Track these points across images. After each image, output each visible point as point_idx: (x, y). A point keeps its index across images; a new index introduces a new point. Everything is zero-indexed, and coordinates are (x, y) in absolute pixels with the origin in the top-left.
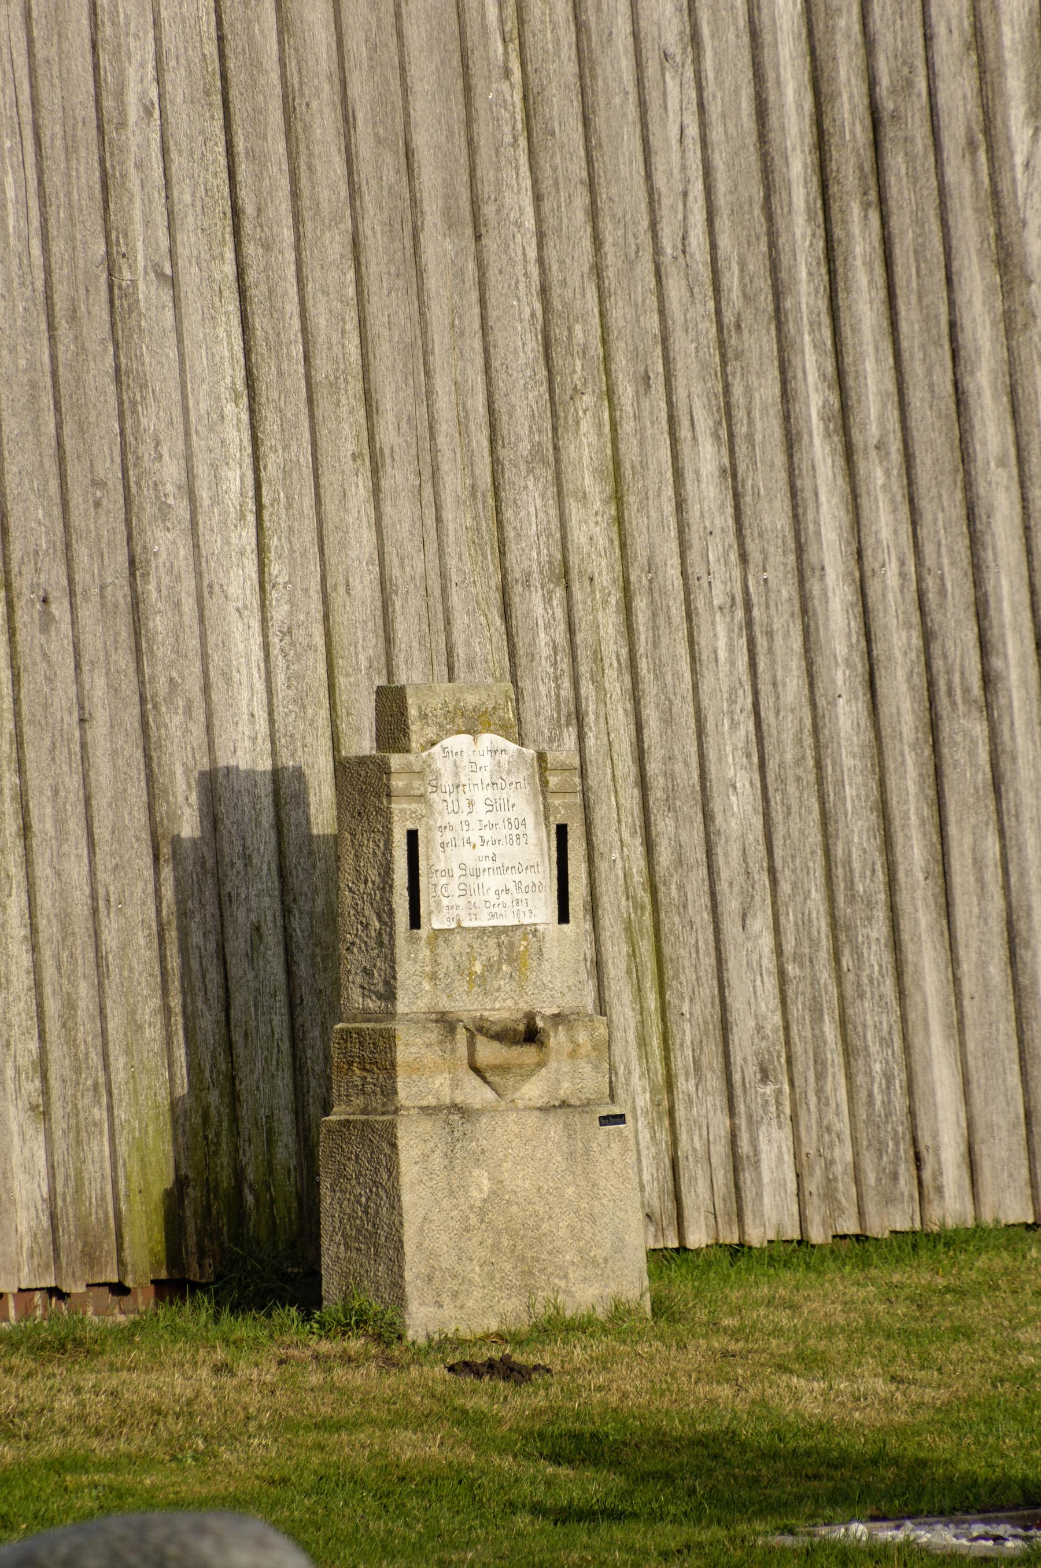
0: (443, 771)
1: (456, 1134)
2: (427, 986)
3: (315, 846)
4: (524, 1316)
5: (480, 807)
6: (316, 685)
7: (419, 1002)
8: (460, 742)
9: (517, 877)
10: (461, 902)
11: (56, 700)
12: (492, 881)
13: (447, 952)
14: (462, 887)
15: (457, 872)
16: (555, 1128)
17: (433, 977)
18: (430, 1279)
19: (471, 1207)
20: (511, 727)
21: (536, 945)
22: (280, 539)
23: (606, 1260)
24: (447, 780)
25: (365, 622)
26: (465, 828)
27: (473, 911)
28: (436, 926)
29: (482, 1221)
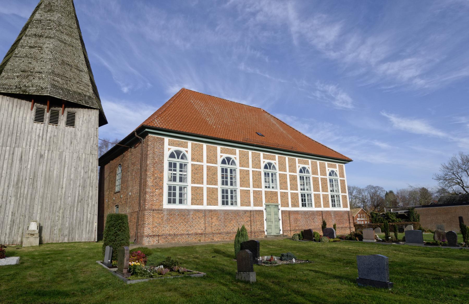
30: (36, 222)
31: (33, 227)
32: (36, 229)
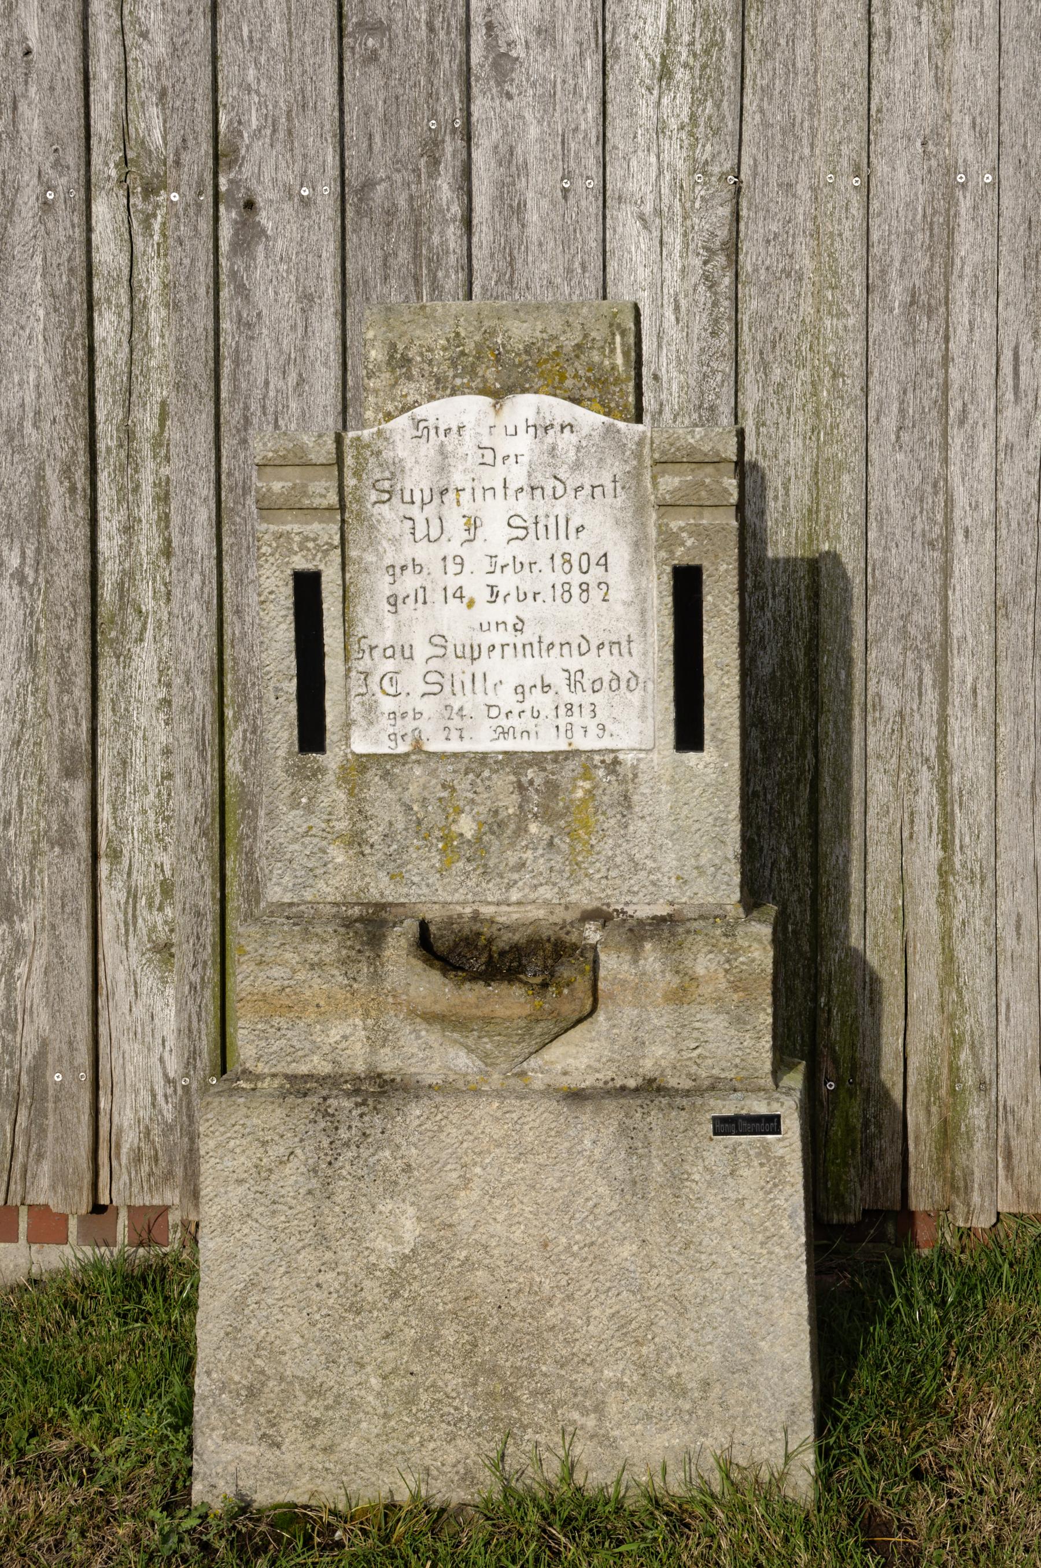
0: (409, 464)
1: (344, 1134)
2: (338, 855)
3: (766, 576)
4: (486, 1475)
5: (495, 533)
7: (321, 884)
8: (468, 409)
9: (574, 663)
10: (429, 706)
11: (257, 355)
12: (508, 671)
13: (389, 795)
14: (432, 678)
16: (595, 1134)
17: (356, 840)
18: (253, 1393)
19: (371, 1269)
20: (617, 381)
21: (615, 788)
22: (718, 105)
23: (706, 1385)
24: (418, 479)
25: (911, 235)
26: (452, 568)
28: (360, 745)
29: (396, 1295)
30: (626, 394)
31: (512, 611)
32: (634, 721)
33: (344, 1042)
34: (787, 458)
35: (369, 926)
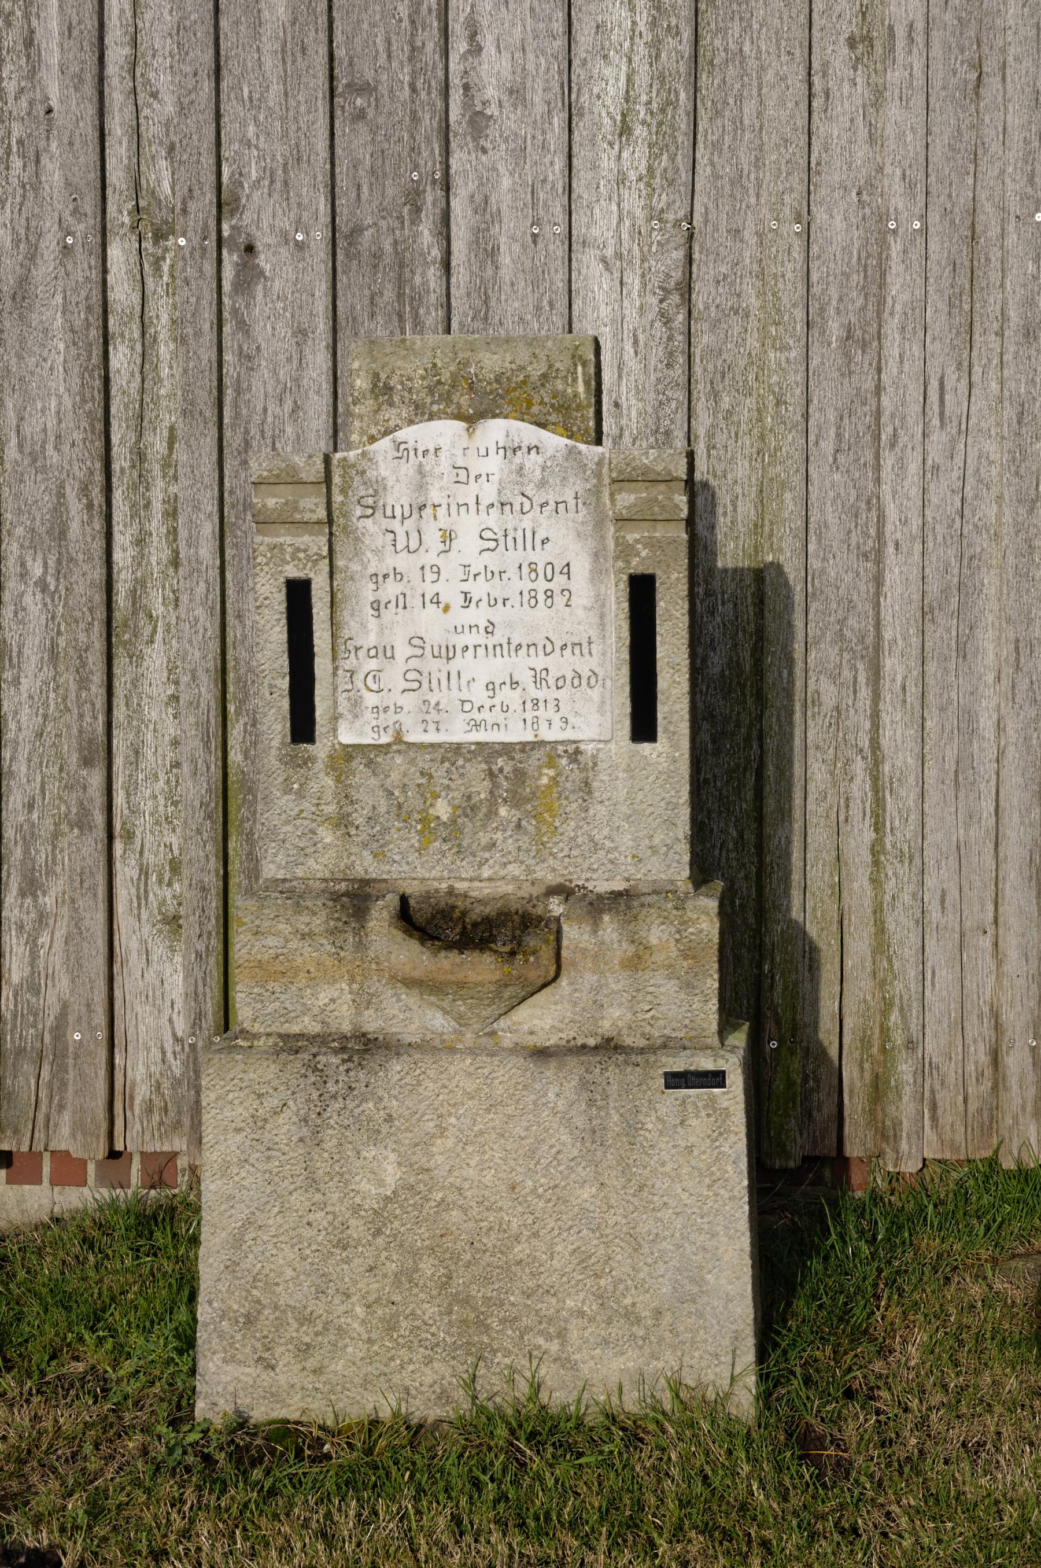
1: (331, 1087)
2: (327, 836)
3: (716, 585)
4: (460, 1395)
5: (468, 545)
6: (742, 363)
7: (311, 862)
8: (444, 432)
9: (540, 662)
12: (480, 668)
13: (373, 781)
15: (403, 651)
17: (342, 822)
18: (250, 1320)
19: (356, 1209)
20: (579, 407)
21: (577, 776)
22: (672, 159)
23: (658, 1313)
24: (398, 496)
25: (847, 276)
26: (430, 576)
27: (433, 715)
28: (347, 736)
30: (583, 416)
31: (484, 614)
32: (592, 714)
33: (332, 1005)
34: (735, 478)
35: (354, 900)
